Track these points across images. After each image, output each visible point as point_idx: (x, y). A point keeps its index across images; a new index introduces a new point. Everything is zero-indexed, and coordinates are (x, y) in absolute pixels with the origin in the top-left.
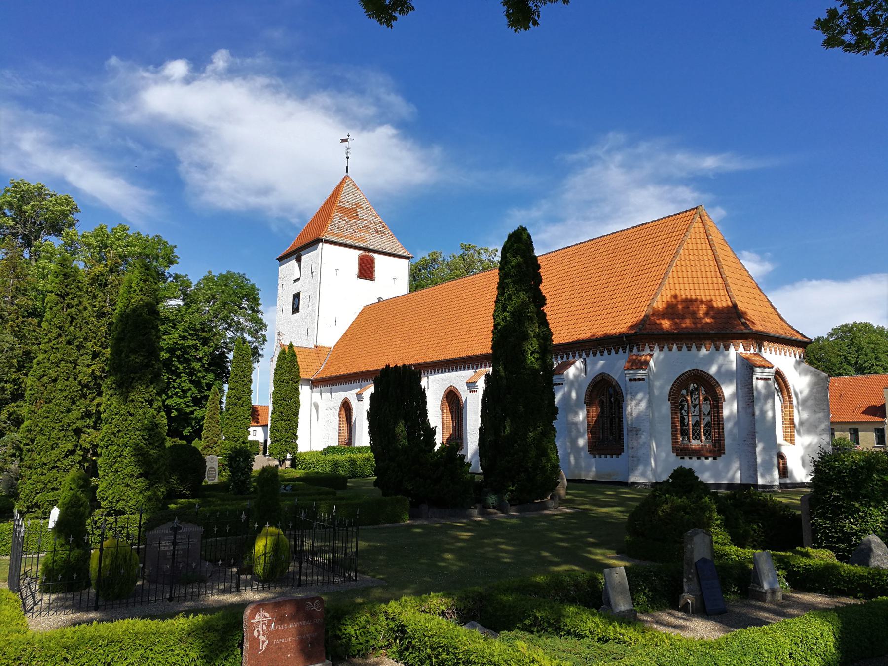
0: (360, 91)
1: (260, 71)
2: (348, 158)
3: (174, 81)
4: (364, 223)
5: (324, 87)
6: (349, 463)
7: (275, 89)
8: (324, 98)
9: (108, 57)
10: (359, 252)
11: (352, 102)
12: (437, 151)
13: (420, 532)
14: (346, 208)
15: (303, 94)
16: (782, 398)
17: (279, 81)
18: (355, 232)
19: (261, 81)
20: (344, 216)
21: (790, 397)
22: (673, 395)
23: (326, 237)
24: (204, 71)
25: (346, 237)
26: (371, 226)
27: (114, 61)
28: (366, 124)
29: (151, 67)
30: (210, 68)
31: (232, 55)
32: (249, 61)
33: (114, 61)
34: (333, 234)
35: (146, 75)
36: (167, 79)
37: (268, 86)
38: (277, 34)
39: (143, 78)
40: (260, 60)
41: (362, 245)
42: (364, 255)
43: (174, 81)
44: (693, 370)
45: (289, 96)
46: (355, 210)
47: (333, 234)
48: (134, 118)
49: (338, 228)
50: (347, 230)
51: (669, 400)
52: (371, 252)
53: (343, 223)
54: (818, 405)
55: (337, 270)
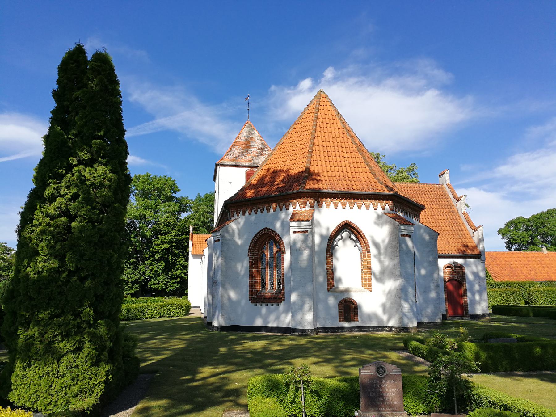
0: (414, 73)
1: (351, 75)
2: (248, 110)
3: (304, 91)
4: (252, 150)
5: (390, 75)
6: (126, 310)
7: (361, 83)
8: (391, 82)
9: (270, 86)
10: (247, 169)
11: (409, 81)
12: (470, 99)
13: (525, 327)
14: (242, 142)
15: (378, 82)
16: (360, 247)
17: (363, 78)
18: (245, 156)
19: (352, 80)
20: (239, 148)
21: (367, 246)
22: (251, 251)
23: (221, 162)
24: (320, 83)
25: (237, 161)
26: (258, 151)
27: (273, 88)
28: (419, 91)
29: (292, 87)
30: (323, 79)
31: (336, 69)
32: (345, 70)
33: (273, 88)
34: (229, 160)
35: (289, 91)
36: (300, 92)
37: (356, 83)
38: (361, 52)
39: (288, 94)
40: (351, 68)
41: (247, 164)
42: (250, 171)
43: (304, 91)
44: (265, 229)
45: (370, 85)
46: (248, 142)
47: (229, 160)
48: (285, 116)
49: (233, 156)
50: (239, 156)
51: (248, 256)
52: (255, 168)
53: (237, 152)
54: (393, 252)
55: (230, 183)
